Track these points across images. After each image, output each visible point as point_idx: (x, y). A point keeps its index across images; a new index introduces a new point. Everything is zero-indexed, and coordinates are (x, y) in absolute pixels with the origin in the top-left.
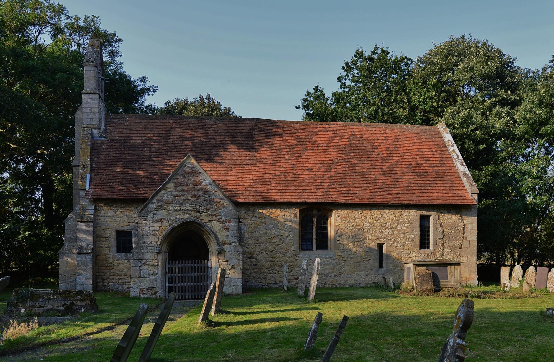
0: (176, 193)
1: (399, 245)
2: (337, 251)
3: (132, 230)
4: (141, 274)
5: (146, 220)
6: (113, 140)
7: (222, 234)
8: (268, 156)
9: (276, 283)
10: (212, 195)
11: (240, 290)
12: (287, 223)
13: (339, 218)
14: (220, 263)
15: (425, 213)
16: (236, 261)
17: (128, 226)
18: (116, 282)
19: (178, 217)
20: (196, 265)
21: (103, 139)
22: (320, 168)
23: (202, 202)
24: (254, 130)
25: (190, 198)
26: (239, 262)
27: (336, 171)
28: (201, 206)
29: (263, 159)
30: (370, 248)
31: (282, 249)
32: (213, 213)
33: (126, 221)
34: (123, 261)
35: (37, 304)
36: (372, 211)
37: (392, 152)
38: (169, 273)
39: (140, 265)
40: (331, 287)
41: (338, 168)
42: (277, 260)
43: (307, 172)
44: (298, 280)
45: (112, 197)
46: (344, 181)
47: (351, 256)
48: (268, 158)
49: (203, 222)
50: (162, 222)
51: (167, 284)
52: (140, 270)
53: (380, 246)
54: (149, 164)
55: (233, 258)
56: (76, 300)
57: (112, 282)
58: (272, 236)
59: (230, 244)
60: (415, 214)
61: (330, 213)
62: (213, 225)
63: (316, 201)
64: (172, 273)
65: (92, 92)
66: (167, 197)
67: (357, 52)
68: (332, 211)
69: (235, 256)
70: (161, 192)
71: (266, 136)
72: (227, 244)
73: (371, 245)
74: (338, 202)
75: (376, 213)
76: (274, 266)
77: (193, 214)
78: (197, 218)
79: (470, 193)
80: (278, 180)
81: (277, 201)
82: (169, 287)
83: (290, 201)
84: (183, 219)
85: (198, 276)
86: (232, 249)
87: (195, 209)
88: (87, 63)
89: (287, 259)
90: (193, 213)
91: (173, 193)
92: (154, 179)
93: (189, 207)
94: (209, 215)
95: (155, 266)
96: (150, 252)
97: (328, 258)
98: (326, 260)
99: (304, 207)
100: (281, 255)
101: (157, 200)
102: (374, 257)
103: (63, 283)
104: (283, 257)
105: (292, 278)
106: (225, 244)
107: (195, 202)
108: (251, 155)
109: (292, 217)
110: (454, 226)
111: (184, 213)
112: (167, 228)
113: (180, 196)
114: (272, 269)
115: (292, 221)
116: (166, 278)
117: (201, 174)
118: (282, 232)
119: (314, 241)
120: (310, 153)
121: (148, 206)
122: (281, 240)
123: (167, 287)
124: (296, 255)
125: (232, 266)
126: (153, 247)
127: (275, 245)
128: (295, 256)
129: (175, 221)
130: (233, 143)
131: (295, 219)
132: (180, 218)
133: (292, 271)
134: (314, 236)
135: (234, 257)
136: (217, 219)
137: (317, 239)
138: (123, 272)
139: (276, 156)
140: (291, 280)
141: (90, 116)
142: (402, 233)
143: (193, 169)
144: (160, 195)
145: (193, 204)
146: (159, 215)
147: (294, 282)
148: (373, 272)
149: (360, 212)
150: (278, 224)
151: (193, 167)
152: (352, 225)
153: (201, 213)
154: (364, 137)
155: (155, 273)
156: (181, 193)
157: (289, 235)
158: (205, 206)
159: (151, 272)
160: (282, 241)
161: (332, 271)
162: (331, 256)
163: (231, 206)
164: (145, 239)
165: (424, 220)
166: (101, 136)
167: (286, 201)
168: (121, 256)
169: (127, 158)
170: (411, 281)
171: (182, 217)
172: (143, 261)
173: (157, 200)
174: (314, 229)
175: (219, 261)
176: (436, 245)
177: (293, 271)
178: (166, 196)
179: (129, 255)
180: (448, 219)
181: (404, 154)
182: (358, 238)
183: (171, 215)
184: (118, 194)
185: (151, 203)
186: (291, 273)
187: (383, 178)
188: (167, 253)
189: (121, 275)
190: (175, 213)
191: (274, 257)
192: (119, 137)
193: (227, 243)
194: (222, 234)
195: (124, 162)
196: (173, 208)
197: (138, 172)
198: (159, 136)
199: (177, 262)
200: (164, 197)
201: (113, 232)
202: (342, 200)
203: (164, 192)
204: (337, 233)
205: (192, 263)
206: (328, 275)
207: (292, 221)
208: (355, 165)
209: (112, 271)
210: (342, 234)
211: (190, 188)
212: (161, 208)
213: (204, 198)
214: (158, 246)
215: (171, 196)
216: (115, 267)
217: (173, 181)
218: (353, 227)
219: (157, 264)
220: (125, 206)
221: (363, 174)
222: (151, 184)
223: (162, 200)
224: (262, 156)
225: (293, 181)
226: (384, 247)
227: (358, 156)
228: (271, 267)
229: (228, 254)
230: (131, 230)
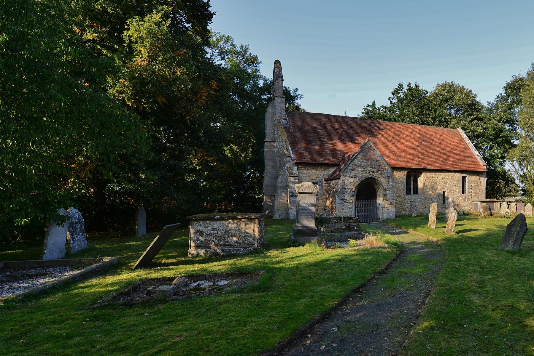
1: (453, 192)
6: (294, 127)
7: (386, 185)
10: (380, 163)
11: (394, 217)
12: (400, 179)
13: (425, 177)
15: (464, 175)
19: (363, 175)
20: (371, 202)
21: (288, 126)
22: (410, 149)
24: (371, 126)
25: (369, 164)
30: (440, 193)
31: (398, 194)
35: (329, 225)
36: (441, 174)
37: (441, 142)
45: (308, 162)
49: (376, 178)
50: (355, 177)
51: (356, 214)
52: (343, 206)
53: (444, 192)
54: (321, 143)
56: (351, 223)
60: (459, 176)
65: (282, 96)
67: (399, 85)
68: (422, 173)
71: (378, 130)
72: (388, 190)
73: (440, 192)
75: (443, 175)
77: (371, 173)
79: (482, 165)
88: (278, 78)
92: (327, 152)
93: (369, 169)
94: (379, 174)
95: (351, 203)
99: (409, 171)
101: (352, 165)
102: (441, 198)
103: (277, 214)
106: (387, 191)
109: (403, 176)
110: (476, 182)
115: (403, 178)
116: (355, 211)
119: (412, 190)
120: (403, 140)
130: (363, 133)
131: (404, 177)
135: (391, 198)
137: (413, 188)
141: (280, 111)
142: (454, 186)
144: (354, 161)
146: (354, 173)
148: (441, 206)
149: (435, 174)
151: (371, 146)
152: (431, 181)
154: (426, 133)
156: (365, 161)
159: (349, 207)
163: (390, 169)
164: (346, 188)
165: (464, 178)
166: (287, 124)
170: (478, 210)
176: (469, 192)
180: (474, 178)
181: (447, 143)
182: (433, 188)
187: (441, 156)
190: (362, 172)
192: (298, 125)
194: (386, 185)
197: (316, 147)
198: (320, 126)
202: (427, 167)
203: (356, 160)
207: (403, 178)
210: (427, 186)
212: (354, 169)
217: (360, 154)
219: (352, 202)
221: (432, 153)
223: (355, 165)
226: (446, 193)
229: (388, 196)
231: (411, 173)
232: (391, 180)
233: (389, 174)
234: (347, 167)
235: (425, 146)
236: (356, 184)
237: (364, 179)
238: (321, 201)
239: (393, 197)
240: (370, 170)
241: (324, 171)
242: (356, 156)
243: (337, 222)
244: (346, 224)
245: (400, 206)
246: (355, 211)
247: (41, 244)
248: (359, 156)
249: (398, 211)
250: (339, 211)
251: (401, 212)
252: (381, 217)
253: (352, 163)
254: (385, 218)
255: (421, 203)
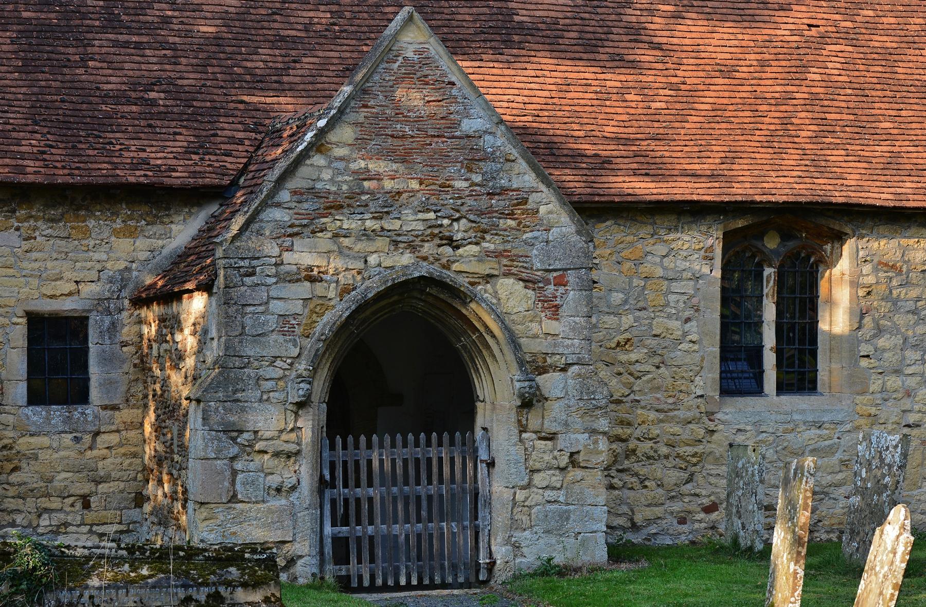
0: (362, 164)
2: (859, 399)
3: (89, 311)
4: (238, 487)
5: (253, 274)
8: (560, 15)
9: (634, 527)
11: (601, 554)
13: (867, 268)
14: (528, 444)
16: (587, 435)
17: (76, 297)
18: (30, 525)
19: (373, 259)
20: (433, 452)
22: (763, 64)
23: (459, 202)
25: (414, 185)
26: (596, 442)
27: (825, 77)
28: (457, 220)
29: (543, 26)
31: (658, 388)
32: (501, 248)
33: (67, 275)
34: (56, 437)
38: (333, 486)
39: (235, 450)
40: (835, 539)
41: (830, 65)
42: (638, 433)
43: (721, 81)
44: (714, 516)
45: (22, 179)
46: (864, 118)
47: (912, 418)
48: (562, 22)
49: (463, 281)
51: (328, 529)
52: (234, 473)
54: (116, 44)
55: (577, 426)
56: (229, 584)
57: (13, 524)
58: (621, 338)
59: (563, 370)
61: (828, 247)
62: (503, 294)
63: (792, 199)
64: (346, 486)
66: (332, 180)
68: (840, 238)
69: (582, 417)
70: (308, 162)
72: (554, 368)
74: (870, 202)
76: (627, 457)
78: (444, 267)
80: (620, 110)
81: (648, 198)
82: (336, 539)
83: (695, 198)
84: (392, 268)
85: (441, 496)
86: (570, 388)
87: (436, 231)
89: (677, 429)
90: (426, 245)
91: (353, 166)
92: (153, 103)
94: (488, 254)
96: (268, 399)
97: (826, 425)
98: (818, 432)
99: (740, 223)
100: (653, 415)
101: (294, 193)
104: (661, 421)
105: (693, 507)
106: (543, 370)
107: (433, 200)
108: (495, 10)
111: (396, 243)
112: (332, 303)
113: (378, 178)
114: (619, 471)
116: (322, 507)
117: (454, 92)
118: (660, 324)
119: (769, 359)
121: (263, 216)
122: (655, 353)
123: (328, 542)
124: (710, 415)
125: (572, 454)
126: (279, 379)
127: (631, 374)
128: (705, 420)
129: (364, 278)
132: (379, 265)
133: (695, 478)
134: (769, 338)
135: (577, 422)
136: (514, 270)
137: (779, 352)
138: (56, 483)
139: (587, 16)
140: (689, 512)
143: (425, 68)
144: (303, 171)
145: (428, 211)
147: (700, 521)
150: (644, 288)
153: (455, 245)
155: (288, 484)
157: (685, 334)
158: (472, 217)
159: (274, 480)
160: (657, 360)
161: (840, 476)
162: (840, 417)
164: (250, 350)
167: (678, 198)
168: (48, 419)
169: (25, 14)
171: (388, 263)
172: (246, 435)
173: (294, 193)
174: (769, 312)
175: (524, 435)
177: (699, 478)
178: (326, 175)
179: (76, 415)
183: (347, 252)
184: (41, 163)
185: (271, 206)
186: (689, 486)
188: (325, 405)
189: (48, 495)
191: (629, 424)
193: (550, 366)
195: (19, 31)
196: (353, 226)
199: (363, 439)
200: (319, 179)
201: (15, 320)
202: (882, 197)
203: (318, 160)
204: (859, 328)
205: (429, 443)
206: (826, 494)
208: (888, 56)
209: (15, 478)
211: (414, 145)
213: (465, 184)
214: (299, 376)
215: (346, 178)
216: (24, 465)
217: (351, 117)
218: (919, 304)
219: (293, 448)
220: (62, 215)
222: (150, 126)
224: (538, 13)
225: (679, 118)
227: (893, 20)
228: (615, 462)
230: (84, 311)
231: (761, 237)
232: (572, 297)
233: (558, 253)
234: (257, 212)
235: (878, 41)
236: (318, 328)
237: (374, 286)
238: (114, 439)
239: (590, 412)
240: (420, 226)
241: (132, 233)
242: (322, 132)
243: (133, 582)
244: (192, 592)
245: (673, 476)
246: (322, 507)
247: (739, 544)
248: (345, 133)
249: (658, 511)
250: (204, 513)
251: (682, 521)
252: (500, 552)
253: (293, 184)
254: (529, 559)
255: (835, 459)
